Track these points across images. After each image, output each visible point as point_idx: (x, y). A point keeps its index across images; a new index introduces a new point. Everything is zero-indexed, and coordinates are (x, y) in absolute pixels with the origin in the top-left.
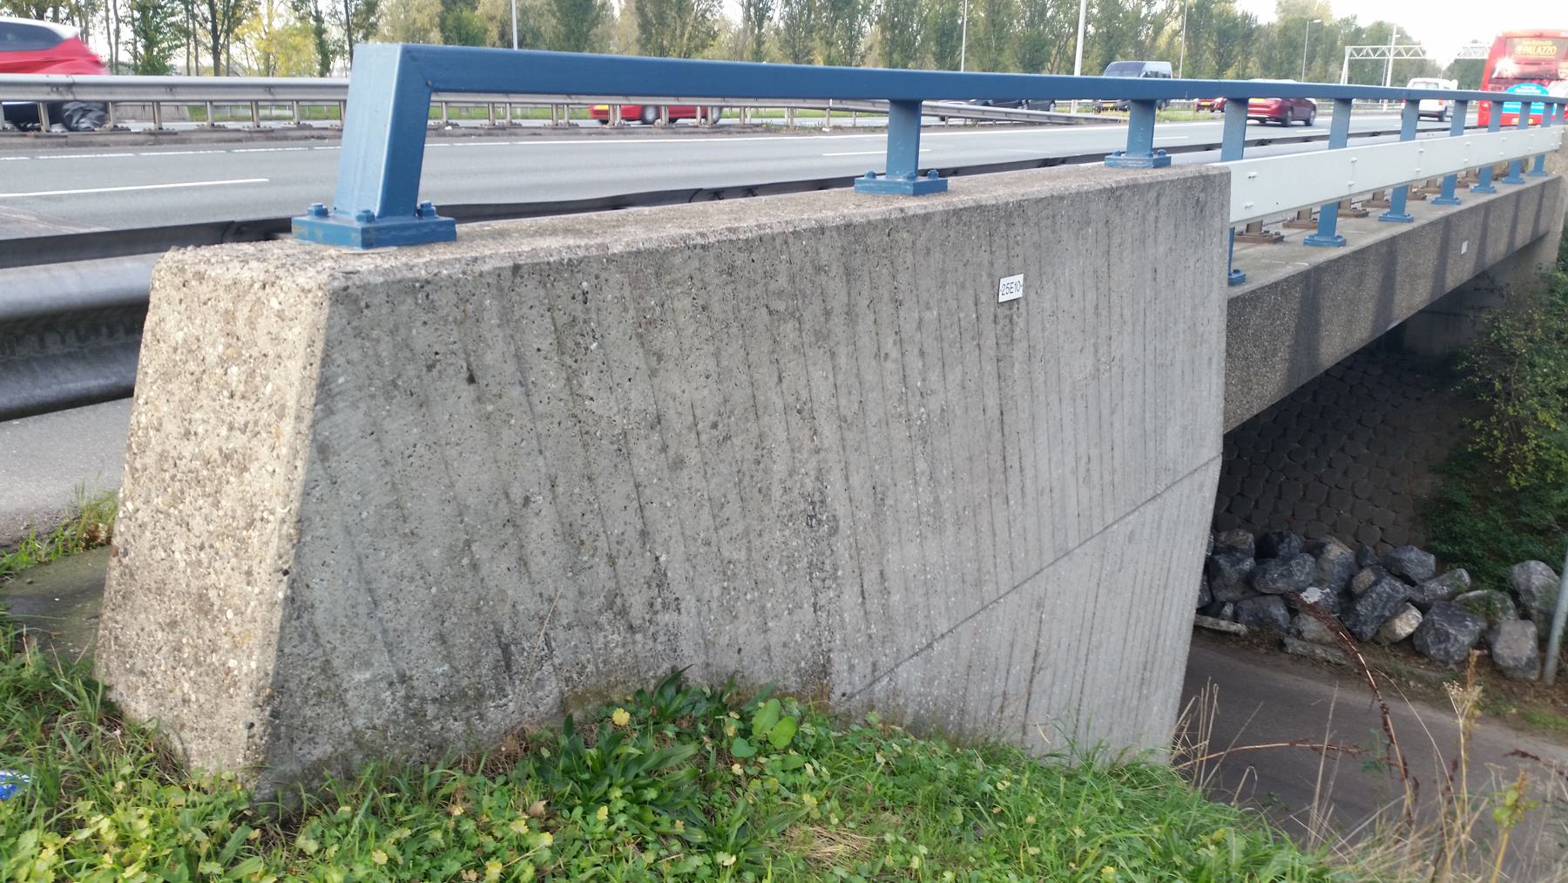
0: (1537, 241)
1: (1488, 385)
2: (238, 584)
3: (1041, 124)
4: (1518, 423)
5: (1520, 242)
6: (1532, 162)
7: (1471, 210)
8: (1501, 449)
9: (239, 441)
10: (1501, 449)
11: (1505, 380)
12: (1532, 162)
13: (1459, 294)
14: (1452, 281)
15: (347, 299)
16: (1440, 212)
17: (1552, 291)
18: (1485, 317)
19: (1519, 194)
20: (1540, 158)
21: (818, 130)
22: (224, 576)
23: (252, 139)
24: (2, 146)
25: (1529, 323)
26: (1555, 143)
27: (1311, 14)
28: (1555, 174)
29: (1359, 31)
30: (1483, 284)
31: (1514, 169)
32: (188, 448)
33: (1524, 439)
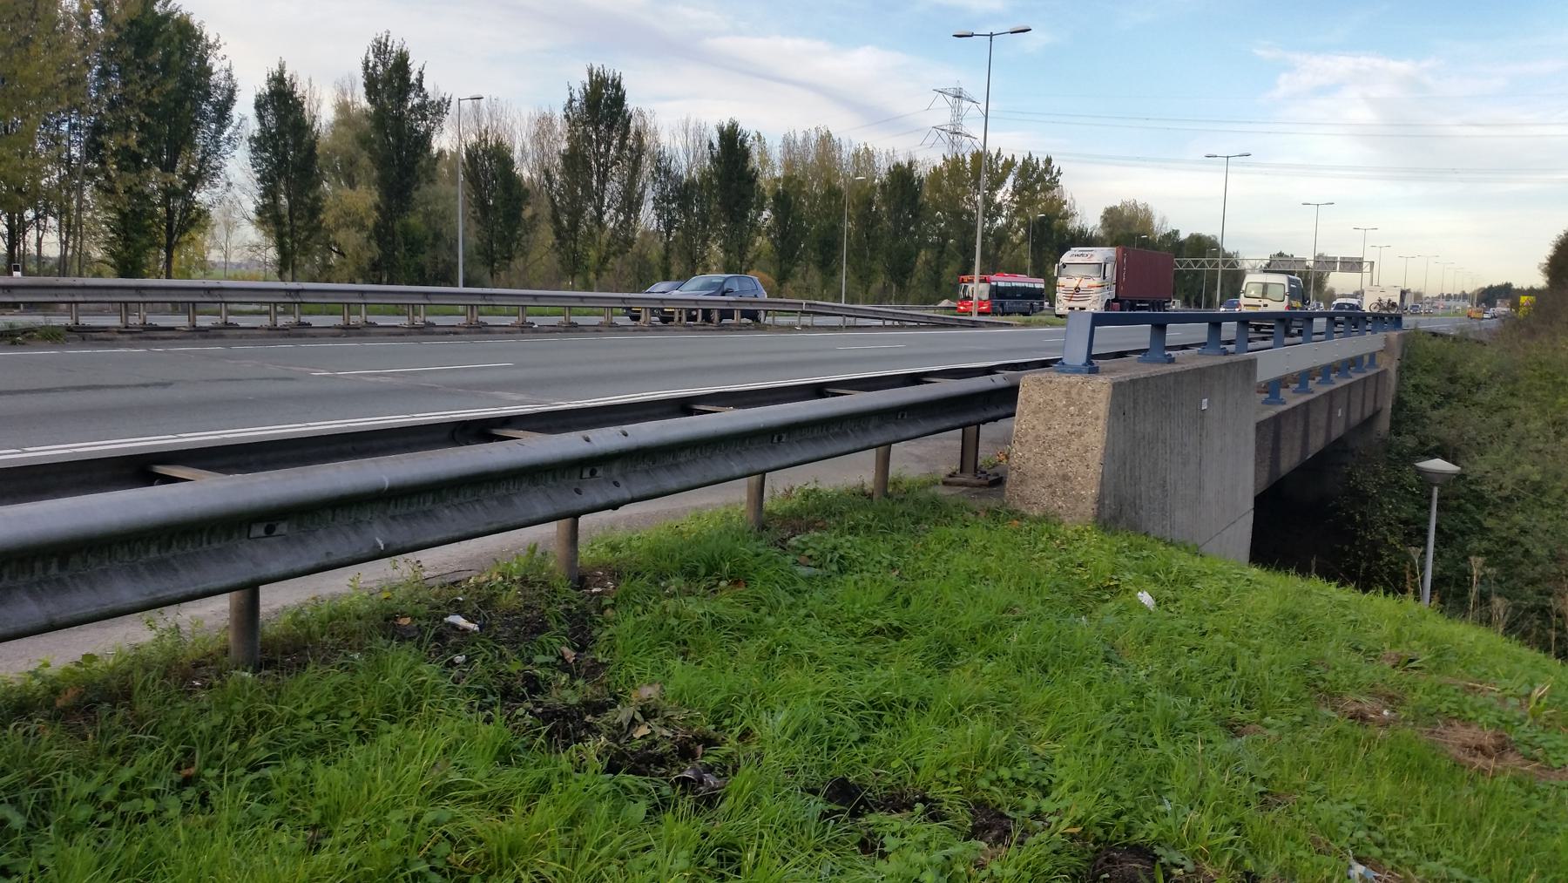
0: (1376, 413)
1: (1351, 518)
2: (1082, 469)
3: (953, 326)
4: (1375, 545)
5: (1368, 413)
6: (1366, 359)
7: (1294, 408)
8: (1364, 565)
9: (1077, 428)
10: (1364, 565)
11: (1362, 514)
12: (1366, 359)
13: (1321, 456)
14: (1334, 436)
15: (1117, 386)
16: (1326, 389)
17: (1389, 451)
18: (1346, 470)
19: (1365, 379)
20: (1372, 356)
21: (790, 328)
22: (1075, 467)
23: (409, 334)
24: (9, 337)
25: (1376, 473)
26: (1381, 346)
27: (1135, 230)
28: (1382, 367)
29: (1182, 244)
30: (1335, 451)
31: (1354, 363)
32: (1050, 433)
33: (1380, 557)
